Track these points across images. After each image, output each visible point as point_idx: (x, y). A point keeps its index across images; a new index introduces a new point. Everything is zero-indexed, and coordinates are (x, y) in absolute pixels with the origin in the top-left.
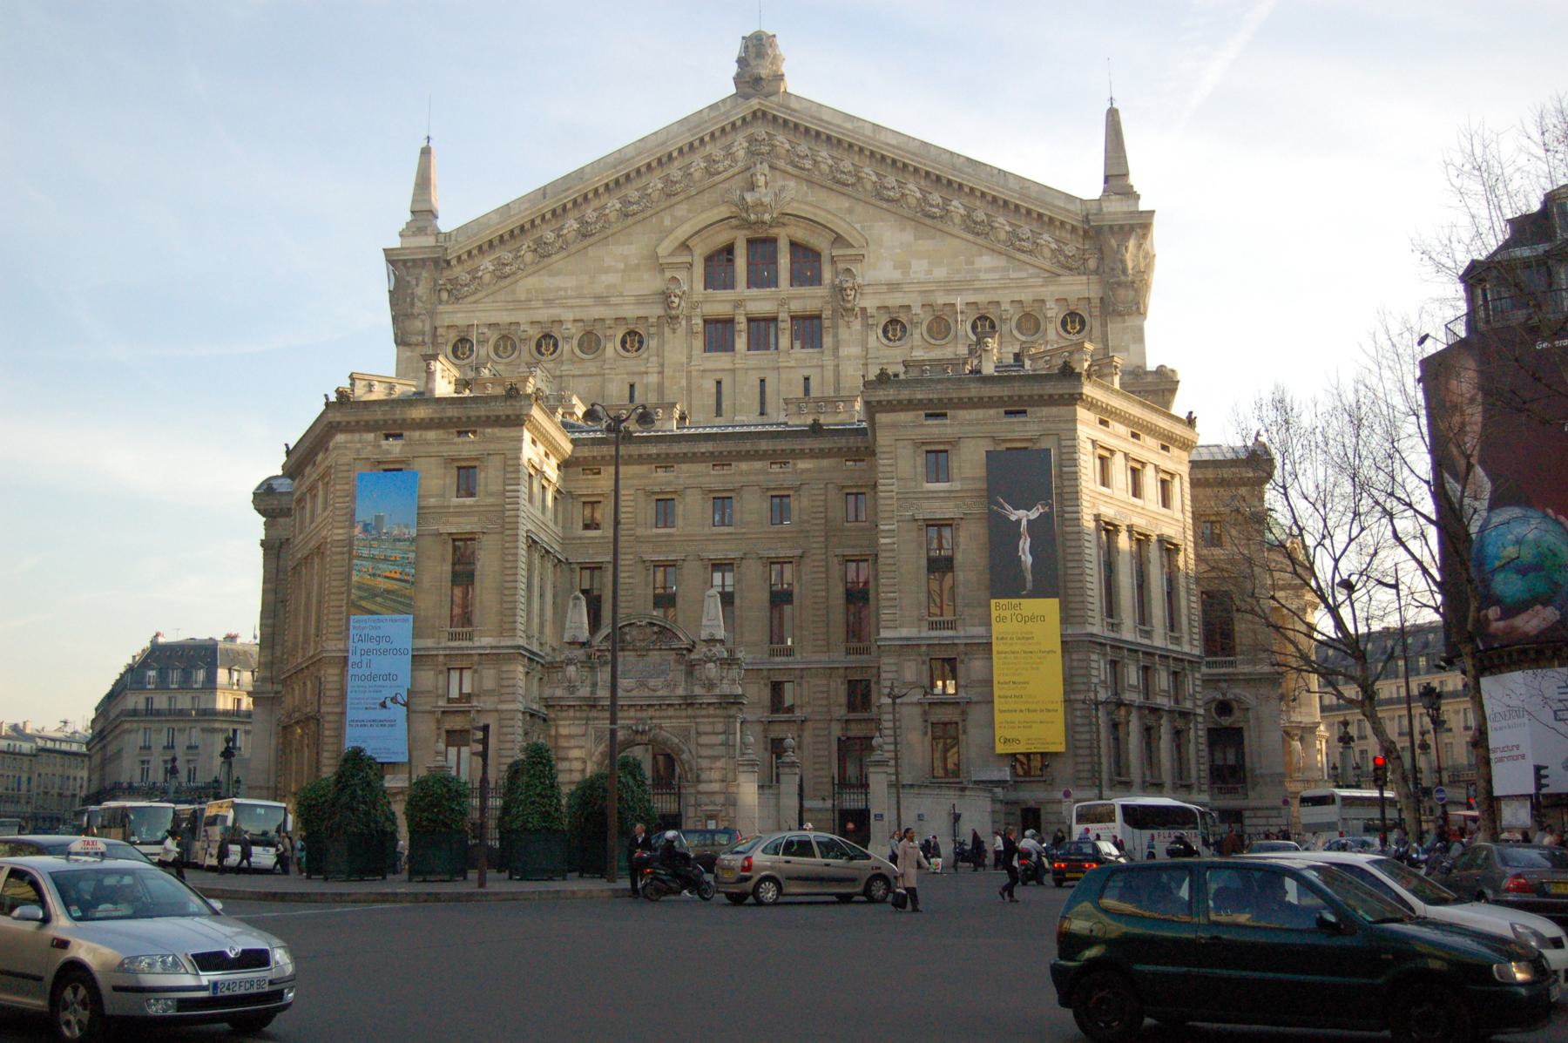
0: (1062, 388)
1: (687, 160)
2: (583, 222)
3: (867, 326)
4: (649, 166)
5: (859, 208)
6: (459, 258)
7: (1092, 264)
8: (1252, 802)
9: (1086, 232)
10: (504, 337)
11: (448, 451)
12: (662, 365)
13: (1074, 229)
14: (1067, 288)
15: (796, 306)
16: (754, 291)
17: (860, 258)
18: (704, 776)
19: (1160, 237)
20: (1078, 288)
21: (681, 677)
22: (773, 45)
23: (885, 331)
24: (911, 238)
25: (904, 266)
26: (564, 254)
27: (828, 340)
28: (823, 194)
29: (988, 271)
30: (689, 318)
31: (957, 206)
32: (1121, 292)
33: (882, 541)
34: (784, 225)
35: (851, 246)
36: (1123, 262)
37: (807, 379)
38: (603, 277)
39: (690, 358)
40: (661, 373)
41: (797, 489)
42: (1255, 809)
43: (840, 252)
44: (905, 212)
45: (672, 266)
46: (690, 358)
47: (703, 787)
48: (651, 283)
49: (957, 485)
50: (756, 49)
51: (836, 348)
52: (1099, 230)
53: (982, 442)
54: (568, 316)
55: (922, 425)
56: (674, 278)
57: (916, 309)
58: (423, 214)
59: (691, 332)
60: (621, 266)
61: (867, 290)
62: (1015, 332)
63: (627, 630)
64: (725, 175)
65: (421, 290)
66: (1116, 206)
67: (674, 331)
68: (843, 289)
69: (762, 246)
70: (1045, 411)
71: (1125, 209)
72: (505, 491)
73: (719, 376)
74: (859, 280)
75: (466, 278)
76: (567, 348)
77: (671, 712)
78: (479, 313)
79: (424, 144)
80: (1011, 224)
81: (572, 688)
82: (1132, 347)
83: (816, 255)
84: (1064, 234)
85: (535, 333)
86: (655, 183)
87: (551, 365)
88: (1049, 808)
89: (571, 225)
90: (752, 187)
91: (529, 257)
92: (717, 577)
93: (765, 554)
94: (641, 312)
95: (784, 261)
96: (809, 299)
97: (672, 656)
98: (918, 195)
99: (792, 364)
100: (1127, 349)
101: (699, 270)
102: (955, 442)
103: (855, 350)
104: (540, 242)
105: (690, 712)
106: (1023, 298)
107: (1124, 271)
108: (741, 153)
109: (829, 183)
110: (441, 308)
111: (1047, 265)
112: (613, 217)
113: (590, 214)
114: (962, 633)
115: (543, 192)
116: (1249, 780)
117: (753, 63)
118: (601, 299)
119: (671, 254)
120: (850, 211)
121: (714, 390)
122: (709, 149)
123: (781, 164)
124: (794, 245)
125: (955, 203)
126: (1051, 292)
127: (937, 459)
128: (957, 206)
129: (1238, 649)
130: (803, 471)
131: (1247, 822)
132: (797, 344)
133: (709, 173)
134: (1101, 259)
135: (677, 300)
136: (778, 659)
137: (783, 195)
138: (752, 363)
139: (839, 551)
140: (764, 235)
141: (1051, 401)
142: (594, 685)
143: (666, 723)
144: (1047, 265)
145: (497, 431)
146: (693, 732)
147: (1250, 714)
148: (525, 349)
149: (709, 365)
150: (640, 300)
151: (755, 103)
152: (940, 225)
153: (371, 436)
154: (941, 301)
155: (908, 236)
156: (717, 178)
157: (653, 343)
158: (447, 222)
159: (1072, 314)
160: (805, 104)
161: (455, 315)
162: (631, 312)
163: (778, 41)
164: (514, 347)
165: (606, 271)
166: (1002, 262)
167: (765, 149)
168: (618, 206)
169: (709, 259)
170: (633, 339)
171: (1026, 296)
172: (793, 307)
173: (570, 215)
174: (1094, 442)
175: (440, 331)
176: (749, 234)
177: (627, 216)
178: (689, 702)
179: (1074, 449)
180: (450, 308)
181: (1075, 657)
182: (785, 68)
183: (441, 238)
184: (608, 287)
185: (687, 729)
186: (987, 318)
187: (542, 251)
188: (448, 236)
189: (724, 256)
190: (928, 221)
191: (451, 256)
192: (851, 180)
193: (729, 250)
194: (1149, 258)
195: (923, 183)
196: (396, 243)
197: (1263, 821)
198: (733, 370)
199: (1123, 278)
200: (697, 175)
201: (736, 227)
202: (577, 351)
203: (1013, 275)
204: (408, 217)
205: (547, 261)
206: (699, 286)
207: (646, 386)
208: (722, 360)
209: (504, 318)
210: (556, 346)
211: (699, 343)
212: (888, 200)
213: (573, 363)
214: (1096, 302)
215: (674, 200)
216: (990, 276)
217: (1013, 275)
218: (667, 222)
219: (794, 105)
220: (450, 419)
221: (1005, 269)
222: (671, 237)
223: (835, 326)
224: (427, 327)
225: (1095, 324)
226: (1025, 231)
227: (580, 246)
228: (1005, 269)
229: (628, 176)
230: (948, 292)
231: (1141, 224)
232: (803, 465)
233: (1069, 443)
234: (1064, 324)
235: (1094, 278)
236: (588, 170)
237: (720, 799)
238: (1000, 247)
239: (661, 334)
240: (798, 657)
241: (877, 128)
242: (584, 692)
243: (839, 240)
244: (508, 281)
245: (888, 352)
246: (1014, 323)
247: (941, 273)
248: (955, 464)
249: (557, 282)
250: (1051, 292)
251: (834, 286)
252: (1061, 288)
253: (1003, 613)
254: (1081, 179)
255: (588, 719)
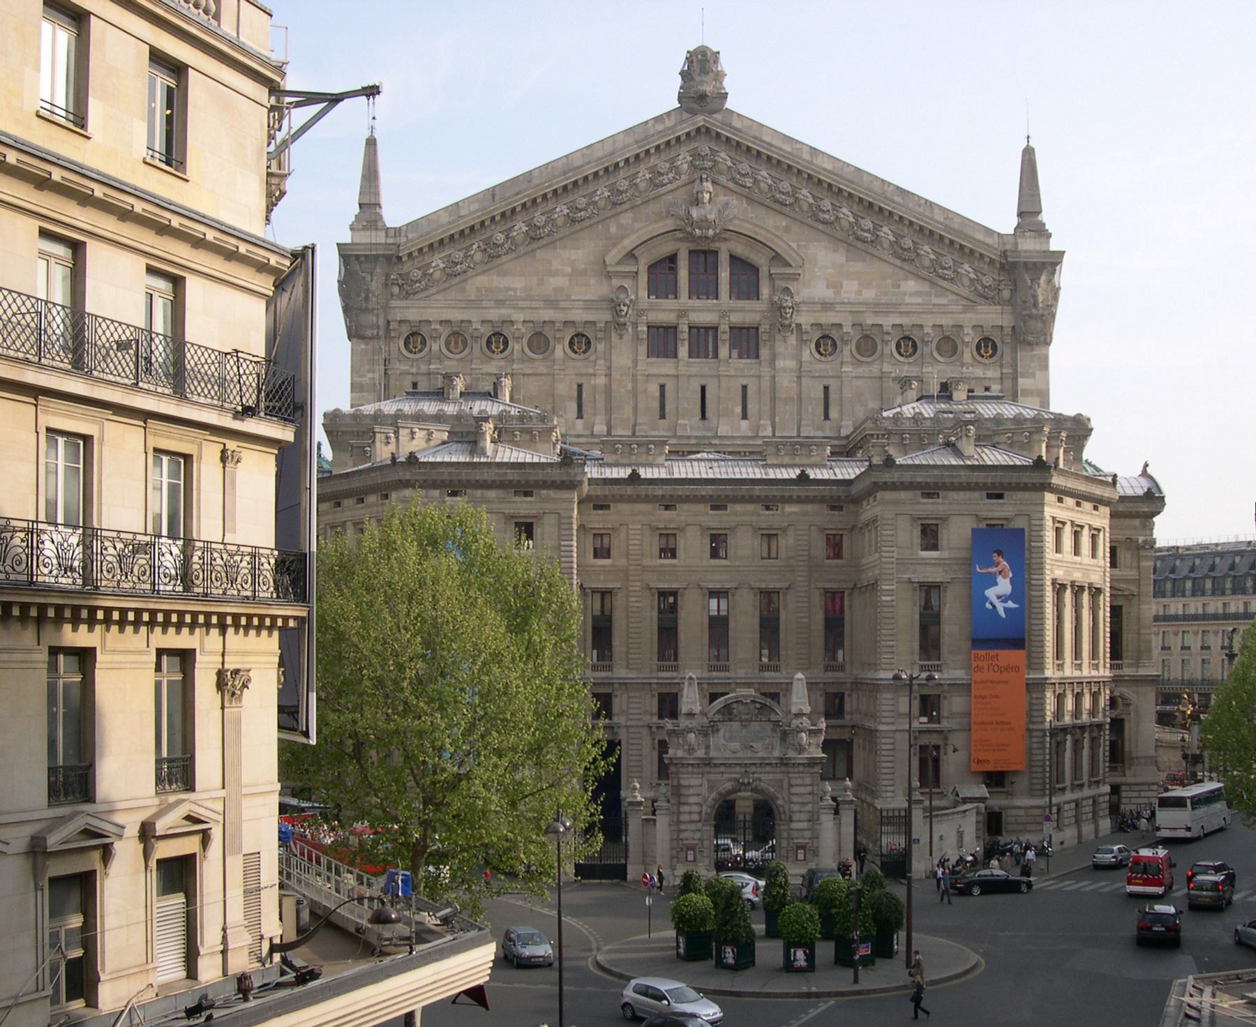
0: (1036, 478)
1: (633, 171)
2: (532, 226)
3: (802, 341)
4: (596, 174)
5: (796, 228)
6: (410, 255)
7: (1006, 294)
8: (1129, 779)
9: (1002, 267)
10: (455, 333)
11: (509, 509)
12: (610, 368)
13: (992, 261)
14: (984, 316)
15: (736, 318)
16: (696, 303)
17: (795, 277)
18: (795, 817)
19: (1066, 277)
20: (993, 316)
21: (777, 742)
22: (716, 61)
23: (818, 346)
24: (843, 259)
25: (836, 286)
26: (514, 255)
27: (764, 352)
28: (762, 212)
29: (911, 295)
30: (635, 325)
31: (886, 232)
32: (1032, 323)
33: (884, 598)
34: (725, 240)
35: (788, 265)
36: (1035, 297)
37: (744, 388)
38: (552, 280)
39: (635, 362)
40: (609, 375)
41: (784, 530)
42: (1130, 784)
43: (780, 270)
44: (839, 235)
45: (619, 274)
46: (635, 362)
47: (794, 825)
48: (597, 289)
49: (946, 554)
50: (700, 68)
51: (773, 358)
52: (1014, 265)
53: (967, 519)
54: (519, 316)
55: (918, 503)
56: (622, 288)
57: (847, 329)
58: (369, 207)
59: (636, 338)
60: (568, 270)
61: (803, 308)
62: (935, 354)
63: (735, 706)
64: (669, 187)
65: (376, 285)
66: (1028, 245)
67: (621, 337)
68: (781, 308)
69: (704, 258)
70: (1020, 495)
71: (1038, 248)
72: (560, 545)
73: (662, 381)
74: (797, 299)
75: (417, 274)
76: (517, 347)
77: (768, 769)
78: (433, 309)
79: (367, 135)
80: (935, 252)
81: (691, 750)
82: (1038, 374)
83: (755, 270)
84: (982, 265)
85: (486, 331)
86: (602, 191)
87: (502, 363)
88: (1010, 812)
89: (520, 227)
90: (697, 201)
91: (478, 257)
92: (713, 603)
93: (757, 585)
94: (589, 317)
95: (724, 275)
96: (748, 312)
97: (769, 726)
98: (851, 219)
99: (732, 373)
100: (1033, 375)
101: (643, 278)
102: (944, 519)
103: (791, 364)
104: (488, 242)
105: (783, 769)
106: (943, 323)
107: (1035, 305)
108: (685, 166)
109: (767, 202)
110: (394, 303)
111: (965, 292)
112: (560, 222)
113: (540, 220)
114: (946, 676)
115: (492, 193)
116: (1127, 762)
117: (698, 78)
118: (551, 303)
119: (618, 263)
120: (787, 229)
121: (658, 394)
122: (653, 160)
123: (723, 180)
124: (733, 258)
125: (885, 229)
126: (968, 319)
127: (930, 535)
128: (886, 232)
129: (1124, 655)
130: (790, 514)
131: (1124, 794)
132: (735, 354)
133: (653, 184)
134: (1014, 291)
135: (625, 309)
136: (766, 674)
137: (717, 206)
138: (693, 370)
139: (821, 585)
140: (706, 248)
141: (1025, 488)
142: (708, 747)
143: (764, 777)
144: (965, 292)
145: (552, 493)
146: (786, 784)
147: (1131, 708)
148: (476, 347)
149: (654, 371)
150: (589, 305)
151: (700, 120)
152: (871, 249)
153: (436, 493)
154: (869, 322)
155: (840, 257)
156: (662, 190)
157: (601, 347)
158: (396, 214)
159: (986, 340)
160: (746, 123)
161: (411, 311)
162: (579, 316)
163: (722, 58)
164: (465, 344)
165: (554, 274)
166: (925, 287)
167: (708, 164)
168: (566, 211)
169: (652, 268)
170: (581, 341)
171: (946, 321)
172: (733, 319)
173: (519, 218)
174: (1054, 518)
175: (393, 325)
176: (693, 247)
177: (573, 221)
178: (784, 762)
179: (1041, 527)
180: (404, 303)
181: (1034, 696)
182: (728, 84)
183: (391, 233)
184: (555, 289)
185: (781, 781)
186: (910, 339)
187: (492, 253)
188: (398, 231)
189: (667, 265)
190: (859, 244)
191: (403, 253)
192: (789, 200)
193: (672, 259)
194: (1055, 292)
195: (855, 207)
196: (347, 238)
197: (1136, 794)
198: (677, 376)
199: (1034, 311)
200: (643, 186)
201: (680, 239)
202: (527, 350)
203: (935, 300)
204: (357, 210)
205: (495, 262)
206: (643, 293)
207: (594, 387)
208: (665, 367)
209: (456, 315)
210: (506, 343)
211: (643, 349)
212: (824, 222)
213: (523, 361)
214: (1008, 331)
215: (619, 209)
216: (913, 299)
217: (935, 300)
218: (613, 230)
219: (736, 123)
220: (510, 481)
221: (929, 294)
222: (620, 247)
223: (772, 339)
224: (381, 322)
225: (1005, 351)
226: (948, 261)
227: (529, 248)
228: (929, 294)
229: (575, 183)
230: (876, 313)
231: (1053, 261)
232: (789, 509)
233: (1037, 522)
234: (978, 348)
235: (1008, 308)
236: (536, 173)
237: (808, 834)
238: (924, 273)
239: (608, 338)
240: (784, 672)
241: (814, 151)
242: (701, 753)
243: (777, 258)
244: (458, 279)
245: (820, 366)
246: (934, 346)
247: (869, 294)
248: (945, 537)
249: (505, 282)
250: (968, 319)
251: (772, 303)
252: (978, 316)
253: (981, 664)
254: (1004, 221)
255: (703, 773)
